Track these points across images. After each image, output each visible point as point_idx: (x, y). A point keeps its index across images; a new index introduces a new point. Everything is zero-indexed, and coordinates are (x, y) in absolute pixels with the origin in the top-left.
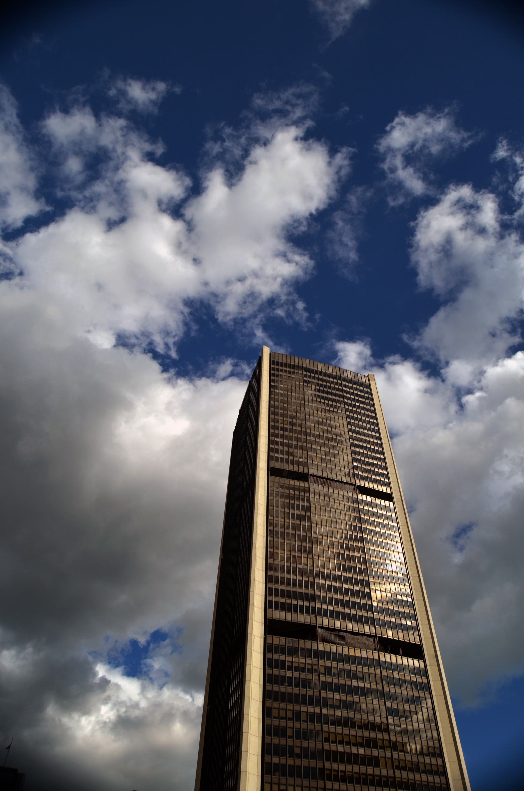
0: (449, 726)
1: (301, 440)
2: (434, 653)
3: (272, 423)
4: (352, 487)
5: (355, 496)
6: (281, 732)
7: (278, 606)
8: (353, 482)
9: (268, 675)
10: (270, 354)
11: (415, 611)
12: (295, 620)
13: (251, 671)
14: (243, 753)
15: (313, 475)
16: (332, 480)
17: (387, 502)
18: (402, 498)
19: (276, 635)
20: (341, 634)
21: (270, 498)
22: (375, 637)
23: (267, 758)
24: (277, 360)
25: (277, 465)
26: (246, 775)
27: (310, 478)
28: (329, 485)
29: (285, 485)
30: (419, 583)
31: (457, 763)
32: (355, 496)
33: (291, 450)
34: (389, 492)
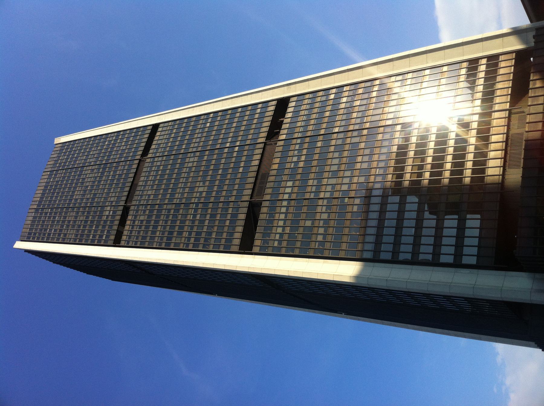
0: (320, 79)
1: (215, 209)
2: (286, 87)
3: (191, 247)
4: (268, 147)
5: (281, 143)
6: (292, 240)
7: (229, 240)
8: (262, 146)
9: (286, 251)
10: (22, 241)
11: (482, 58)
12: (242, 223)
13: (281, 270)
14: (334, 280)
15: (252, 196)
16: (133, 182)
17: (291, 105)
18: (196, 106)
19: (253, 243)
20: (259, 177)
21: (181, 248)
22: (510, 111)
23: (342, 254)
24: (27, 234)
25: (237, 242)
26: (371, 279)
27: (256, 199)
28: (137, 185)
29: (130, 229)
30: (227, 101)
31: (464, 47)
32: (281, 143)
33: (102, 223)
34: (274, 103)
